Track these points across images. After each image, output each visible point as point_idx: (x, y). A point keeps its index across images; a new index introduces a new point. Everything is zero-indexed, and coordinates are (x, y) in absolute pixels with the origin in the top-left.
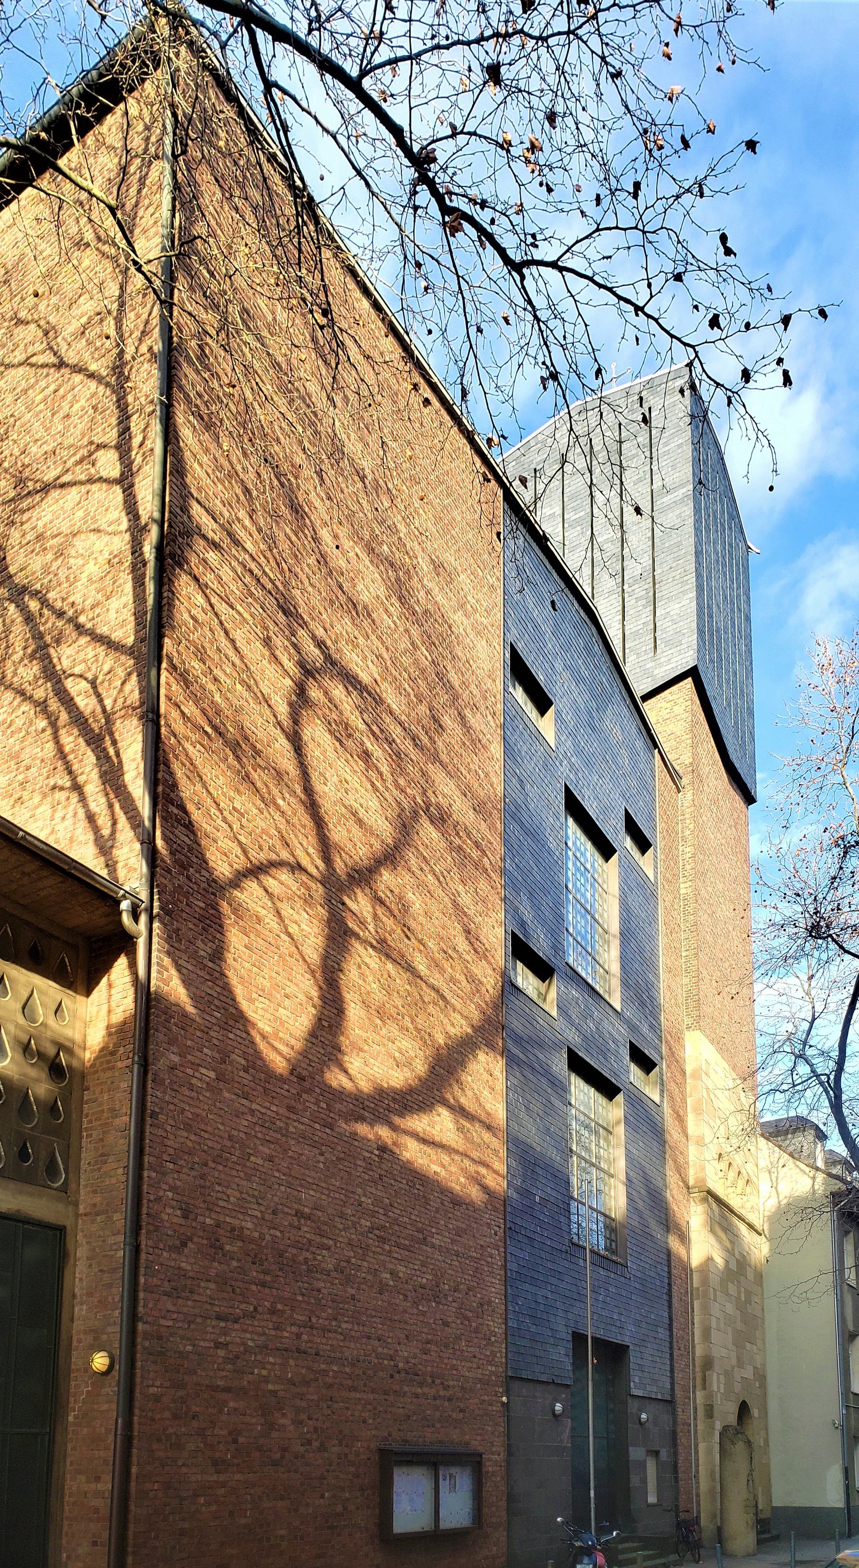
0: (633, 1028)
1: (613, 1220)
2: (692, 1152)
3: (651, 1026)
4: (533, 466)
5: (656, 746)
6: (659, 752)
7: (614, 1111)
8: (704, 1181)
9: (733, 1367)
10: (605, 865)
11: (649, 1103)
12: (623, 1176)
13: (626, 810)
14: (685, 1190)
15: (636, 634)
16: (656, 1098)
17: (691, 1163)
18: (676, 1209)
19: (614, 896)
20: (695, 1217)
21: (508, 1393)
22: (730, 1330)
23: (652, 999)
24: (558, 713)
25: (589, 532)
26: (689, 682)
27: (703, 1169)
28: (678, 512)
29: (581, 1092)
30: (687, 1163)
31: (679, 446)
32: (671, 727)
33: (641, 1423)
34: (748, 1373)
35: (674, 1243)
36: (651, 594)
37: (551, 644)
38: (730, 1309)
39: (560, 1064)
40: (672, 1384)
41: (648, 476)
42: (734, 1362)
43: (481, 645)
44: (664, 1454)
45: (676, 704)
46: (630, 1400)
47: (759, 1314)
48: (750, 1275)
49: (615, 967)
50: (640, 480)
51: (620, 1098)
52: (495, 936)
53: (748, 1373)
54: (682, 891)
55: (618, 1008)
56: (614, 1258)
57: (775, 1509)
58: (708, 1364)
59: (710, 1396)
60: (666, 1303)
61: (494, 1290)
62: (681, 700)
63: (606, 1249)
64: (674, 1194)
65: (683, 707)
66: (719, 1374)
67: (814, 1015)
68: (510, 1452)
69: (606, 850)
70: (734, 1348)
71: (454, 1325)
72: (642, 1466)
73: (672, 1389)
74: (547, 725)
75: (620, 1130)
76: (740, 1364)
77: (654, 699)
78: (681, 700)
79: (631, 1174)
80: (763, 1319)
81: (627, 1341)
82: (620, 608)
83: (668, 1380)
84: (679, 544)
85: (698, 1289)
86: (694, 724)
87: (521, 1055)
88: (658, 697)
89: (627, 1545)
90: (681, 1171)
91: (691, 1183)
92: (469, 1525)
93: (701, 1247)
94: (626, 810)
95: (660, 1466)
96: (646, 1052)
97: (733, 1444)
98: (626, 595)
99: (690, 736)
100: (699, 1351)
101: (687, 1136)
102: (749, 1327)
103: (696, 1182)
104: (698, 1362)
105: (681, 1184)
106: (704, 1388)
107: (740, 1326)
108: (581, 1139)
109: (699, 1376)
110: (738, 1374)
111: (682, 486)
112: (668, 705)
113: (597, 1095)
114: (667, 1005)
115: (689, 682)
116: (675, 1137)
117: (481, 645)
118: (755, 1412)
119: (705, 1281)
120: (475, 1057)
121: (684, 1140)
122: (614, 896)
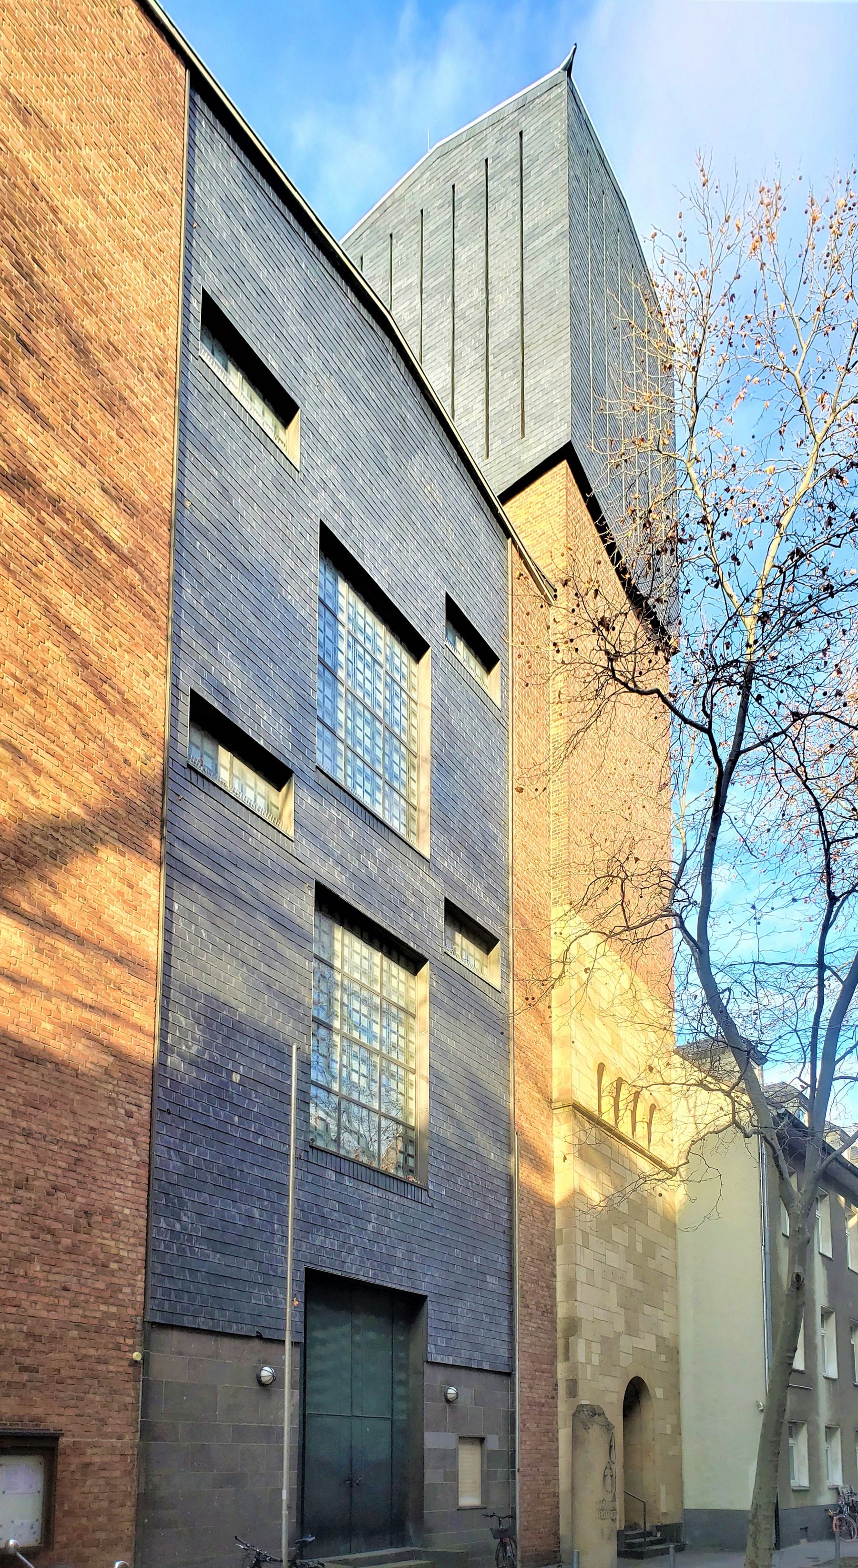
0: (448, 880)
1: (413, 1129)
2: (557, 1059)
3: (489, 889)
4: (389, 232)
5: (508, 534)
6: (514, 542)
7: (418, 988)
8: (570, 1091)
9: (619, 1335)
10: (414, 667)
11: (486, 989)
12: (425, 1071)
13: (448, 597)
14: (544, 1104)
15: (501, 413)
16: (497, 983)
17: (555, 1072)
18: (526, 1125)
19: (426, 707)
20: (559, 1138)
21: (146, 1345)
22: (613, 1287)
23: (492, 856)
24: (307, 421)
25: (450, 300)
26: (563, 467)
27: (569, 1078)
28: (550, 256)
29: (350, 952)
30: (550, 1071)
31: (555, 173)
32: (542, 525)
33: (448, 1401)
34: (648, 1343)
35: (525, 1174)
36: (519, 362)
37: (294, 328)
38: (614, 1259)
39: (302, 906)
40: (512, 1350)
41: (518, 217)
42: (620, 1326)
43: (132, 271)
44: (493, 1443)
45: (548, 496)
46: (428, 1370)
47: (668, 1269)
48: (654, 1222)
49: (424, 801)
50: (509, 224)
51: (425, 970)
52: (152, 688)
53: (648, 1343)
54: (552, 732)
55: (427, 855)
56: (412, 1179)
57: (686, 1512)
58: (573, 1326)
59: (573, 1369)
60: (503, 1245)
61: (126, 1197)
62: (555, 489)
63: (398, 1166)
64: (523, 1104)
65: (557, 498)
66: (589, 1342)
67: (685, 854)
68: (147, 1431)
69: (416, 646)
70: (621, 1311)
71: (12, 1238)
72: (450, 1458)
73: (512, 1358)
74: (290, 439)
75: (424, 1012)
76: (631, 1330)
77: (523, 494)
78: (555, 489)
79: (436, 1065)
80: (676, 1278)
81: (422, 1289)
82: (484, 385)
83: (505, 1346)
84: (551, 296)
85: (561, 1230)
86: (569, 521)
87: (219, 881)
88: (528, 490)
89: (638, 1540)
90: (540, 1081)
91: (555, 1096)
92: (36, 1544)
93: (568, 1178)
94: (448, 597)
95: (489, 1459)
96: (478, 919)
97: (586, 1428)
98: (491, 368)
99: (564, 533)
100: (561, 1311)
101: (550, 1038)
102: (650, 1283)
103: (560, 1094)
104: (560, 1326)
105: (538, 1096)
106: (567, 1358)
107: (631, 1282)
108: (351, 1017)
109: (560, 1343)
110: (626, 1343)
111: (557, 221)
112: (540, 499)
113: (386, 962)
114: (517, 868)
115: (563, 467)
116: (527, 1035)
117: (132, 271)
118: (657, 1392)
119: (570, 1220)
120: (94, 852)
121: (545, 1041)
122: (426, 707)
